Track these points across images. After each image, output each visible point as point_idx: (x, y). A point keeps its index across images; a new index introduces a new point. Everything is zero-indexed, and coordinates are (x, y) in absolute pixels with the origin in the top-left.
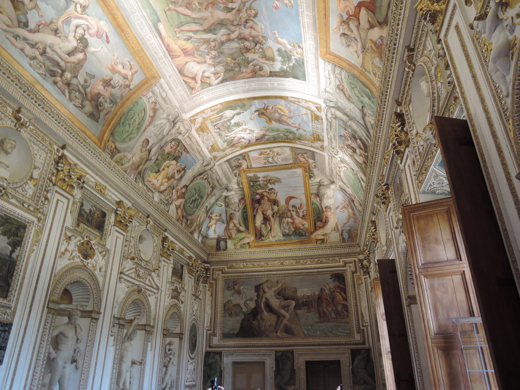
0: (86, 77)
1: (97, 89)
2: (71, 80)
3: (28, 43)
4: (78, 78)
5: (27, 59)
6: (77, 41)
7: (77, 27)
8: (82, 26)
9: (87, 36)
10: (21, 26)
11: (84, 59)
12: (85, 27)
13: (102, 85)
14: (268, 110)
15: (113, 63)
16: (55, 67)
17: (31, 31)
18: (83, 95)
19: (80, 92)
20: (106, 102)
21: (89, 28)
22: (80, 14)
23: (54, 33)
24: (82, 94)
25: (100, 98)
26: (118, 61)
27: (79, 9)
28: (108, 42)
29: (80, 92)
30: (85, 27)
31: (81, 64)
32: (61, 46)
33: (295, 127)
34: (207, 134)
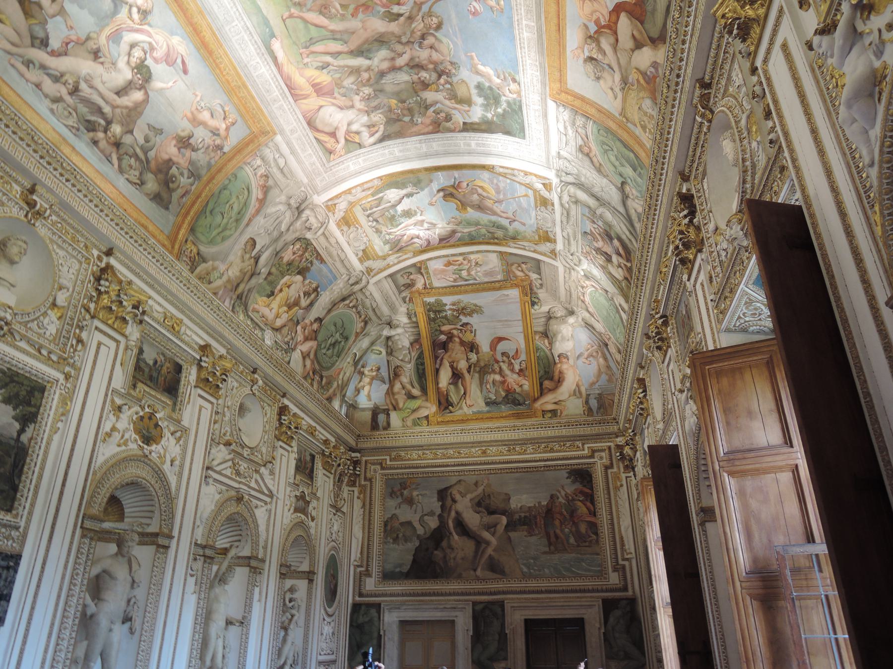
0: (147, 131)
1: (167, 153)
2: (121, 137)
3: (48, 75)
4: (134, 133)
5: (47, 102)
6: (133, 70)
7: (132, 46)
8: (141, 45)
9: (149, 62)
10: (36, 45)
11: (144, 101)
12: (146, 47)
13: (175, 146)
14: (461, 188)
15: (193, 109)
16: (94, 116)
17: (53, 53)
18: (143, 162)
19: (137, 157)
20: (182, 174)
21: (152, 48)
22: (138, 24)
23: (92, 56)
24: (141, 161)
25: (171, 168)
26: (203, 104)
27: (136, 16)
28: (185, 72)
29: (137, 157)
30: (146, 47)
31: (139, 109)
32: (104, 79)
33: (507, 218)
34: (355, 229)
